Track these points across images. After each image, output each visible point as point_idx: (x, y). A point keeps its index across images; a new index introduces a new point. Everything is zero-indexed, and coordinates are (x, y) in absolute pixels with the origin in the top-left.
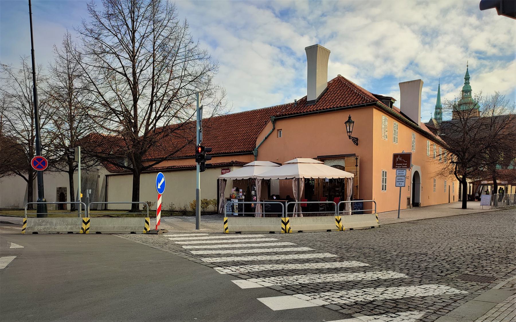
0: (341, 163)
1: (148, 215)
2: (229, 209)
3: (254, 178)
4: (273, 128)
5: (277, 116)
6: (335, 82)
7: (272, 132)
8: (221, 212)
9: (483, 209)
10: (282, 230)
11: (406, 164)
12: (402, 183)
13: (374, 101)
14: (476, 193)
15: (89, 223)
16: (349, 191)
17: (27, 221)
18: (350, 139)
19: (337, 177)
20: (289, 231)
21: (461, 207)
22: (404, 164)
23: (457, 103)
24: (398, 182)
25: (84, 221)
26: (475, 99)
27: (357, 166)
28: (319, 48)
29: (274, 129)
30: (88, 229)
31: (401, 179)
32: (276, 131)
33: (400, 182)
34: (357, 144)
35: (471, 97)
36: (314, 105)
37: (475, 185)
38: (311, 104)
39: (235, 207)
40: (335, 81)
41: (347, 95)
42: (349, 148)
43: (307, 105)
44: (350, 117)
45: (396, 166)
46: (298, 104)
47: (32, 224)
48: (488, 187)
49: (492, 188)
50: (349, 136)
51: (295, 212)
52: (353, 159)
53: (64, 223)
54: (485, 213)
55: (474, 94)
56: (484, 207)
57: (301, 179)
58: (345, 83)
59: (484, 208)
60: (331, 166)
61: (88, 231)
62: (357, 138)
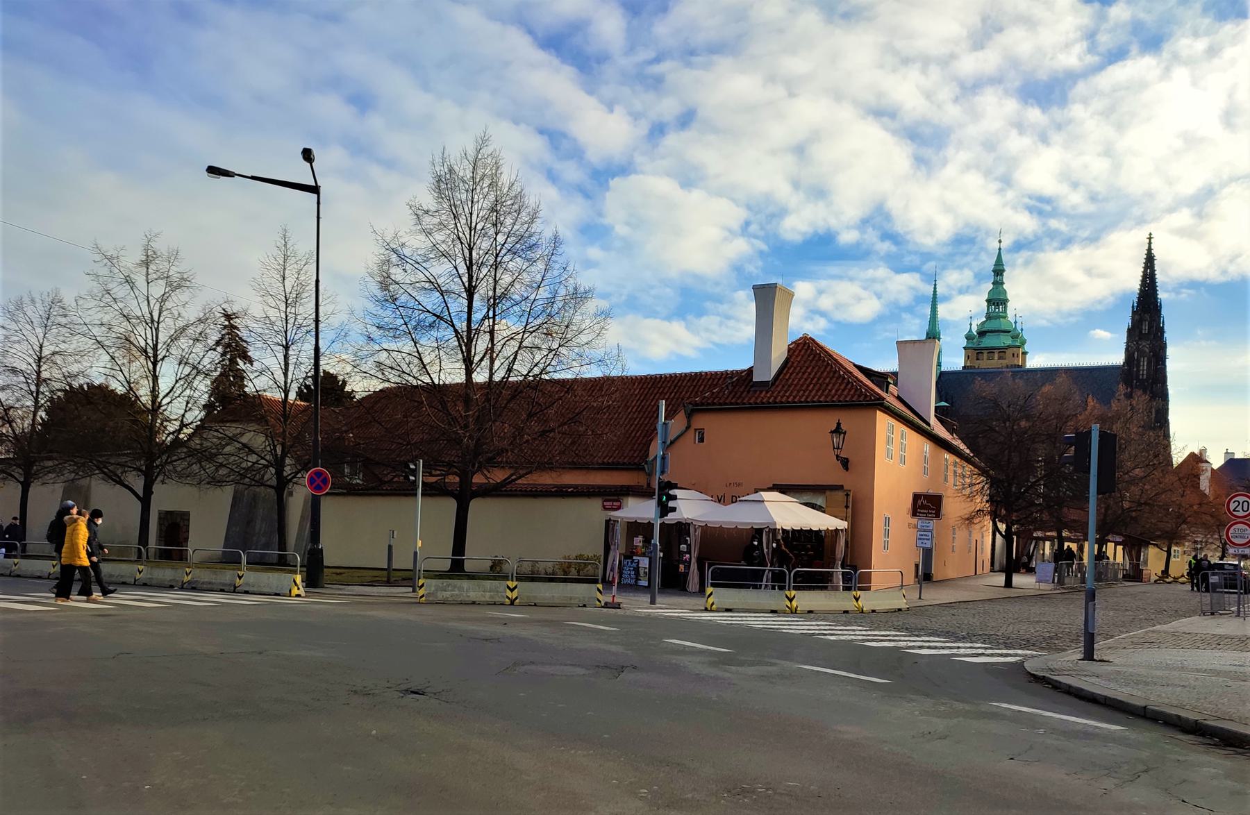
0: (820, 501)
1: (600, 581)
2: (630, 575)
3: (686, 523)
4: (686, 425)
5: (697, 405)
6: (800, 348)
7: (685, 431)
8: (610, 580)
9: (1039, 589)
10: (787, 609)
11: (934, 512)
12: (926, 541)
13: (878, 399)
14: (1023, 555)
15: (516, 590)
16: (840, 553)
17: (425, 585)
18: (838, 460)
19: (825, 528)
20: (796, 610)
21: (1003, 584)
22: (930, 511)
23: (975, 330)
24: (920, 539)
25: (508, 587)
26: (1016, 322)
27: (847, 507)
28: (778, 289)
29: (688, 428)
30: (516, 598)
31: (926, 535)
32: (691, 431)
33: (924, 539)
34: (847, 469)
35: (1005, 317)
36: (767, 392)
37: (1021, 539)
38: (761, 389)
39: (642, 572)
40: (798, 346)
41: (828, 380)
42: (833, 475)
43: (752, 389)
44: (839, 424)
45: (918, 514)
46: (734, 384)
47: (433, 589)
48: (1044, 543)
49: (1052, 545)
50: (837, 456)
51: (767, 582)
52: (840, 495)
53: (479, 588)
54: (1045, 596)
55: (1016, 308)
56: (1043, 586)
57: (779, 530)
58: (820, 354)
59: (1041, 588)
60: (801, 504)
61: (517, 601)
62: (847, 459)
